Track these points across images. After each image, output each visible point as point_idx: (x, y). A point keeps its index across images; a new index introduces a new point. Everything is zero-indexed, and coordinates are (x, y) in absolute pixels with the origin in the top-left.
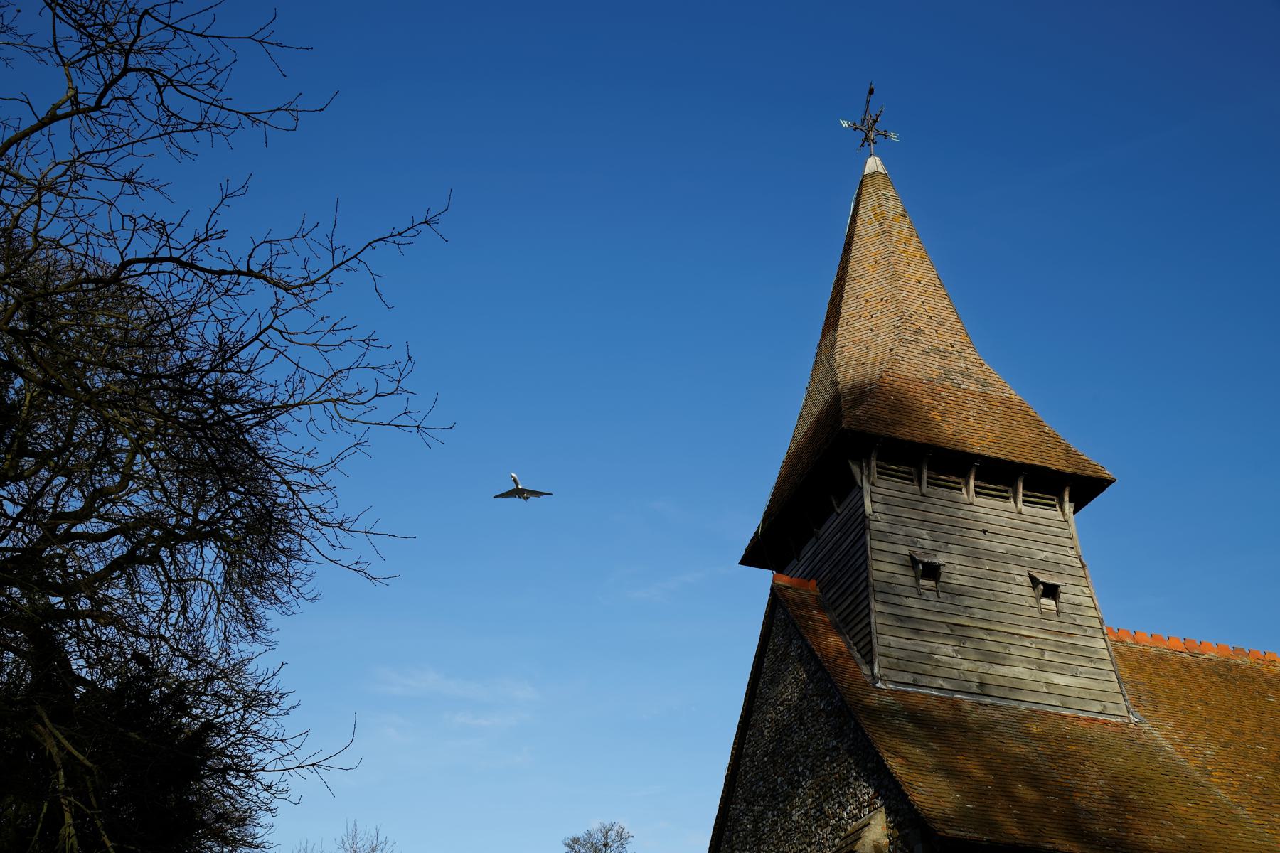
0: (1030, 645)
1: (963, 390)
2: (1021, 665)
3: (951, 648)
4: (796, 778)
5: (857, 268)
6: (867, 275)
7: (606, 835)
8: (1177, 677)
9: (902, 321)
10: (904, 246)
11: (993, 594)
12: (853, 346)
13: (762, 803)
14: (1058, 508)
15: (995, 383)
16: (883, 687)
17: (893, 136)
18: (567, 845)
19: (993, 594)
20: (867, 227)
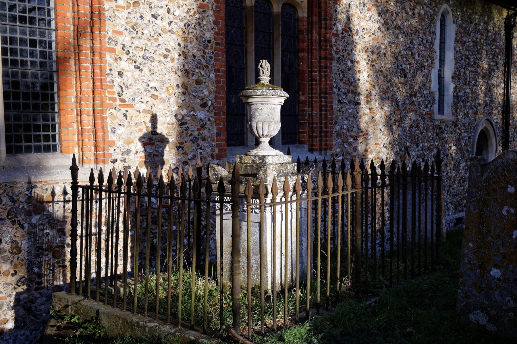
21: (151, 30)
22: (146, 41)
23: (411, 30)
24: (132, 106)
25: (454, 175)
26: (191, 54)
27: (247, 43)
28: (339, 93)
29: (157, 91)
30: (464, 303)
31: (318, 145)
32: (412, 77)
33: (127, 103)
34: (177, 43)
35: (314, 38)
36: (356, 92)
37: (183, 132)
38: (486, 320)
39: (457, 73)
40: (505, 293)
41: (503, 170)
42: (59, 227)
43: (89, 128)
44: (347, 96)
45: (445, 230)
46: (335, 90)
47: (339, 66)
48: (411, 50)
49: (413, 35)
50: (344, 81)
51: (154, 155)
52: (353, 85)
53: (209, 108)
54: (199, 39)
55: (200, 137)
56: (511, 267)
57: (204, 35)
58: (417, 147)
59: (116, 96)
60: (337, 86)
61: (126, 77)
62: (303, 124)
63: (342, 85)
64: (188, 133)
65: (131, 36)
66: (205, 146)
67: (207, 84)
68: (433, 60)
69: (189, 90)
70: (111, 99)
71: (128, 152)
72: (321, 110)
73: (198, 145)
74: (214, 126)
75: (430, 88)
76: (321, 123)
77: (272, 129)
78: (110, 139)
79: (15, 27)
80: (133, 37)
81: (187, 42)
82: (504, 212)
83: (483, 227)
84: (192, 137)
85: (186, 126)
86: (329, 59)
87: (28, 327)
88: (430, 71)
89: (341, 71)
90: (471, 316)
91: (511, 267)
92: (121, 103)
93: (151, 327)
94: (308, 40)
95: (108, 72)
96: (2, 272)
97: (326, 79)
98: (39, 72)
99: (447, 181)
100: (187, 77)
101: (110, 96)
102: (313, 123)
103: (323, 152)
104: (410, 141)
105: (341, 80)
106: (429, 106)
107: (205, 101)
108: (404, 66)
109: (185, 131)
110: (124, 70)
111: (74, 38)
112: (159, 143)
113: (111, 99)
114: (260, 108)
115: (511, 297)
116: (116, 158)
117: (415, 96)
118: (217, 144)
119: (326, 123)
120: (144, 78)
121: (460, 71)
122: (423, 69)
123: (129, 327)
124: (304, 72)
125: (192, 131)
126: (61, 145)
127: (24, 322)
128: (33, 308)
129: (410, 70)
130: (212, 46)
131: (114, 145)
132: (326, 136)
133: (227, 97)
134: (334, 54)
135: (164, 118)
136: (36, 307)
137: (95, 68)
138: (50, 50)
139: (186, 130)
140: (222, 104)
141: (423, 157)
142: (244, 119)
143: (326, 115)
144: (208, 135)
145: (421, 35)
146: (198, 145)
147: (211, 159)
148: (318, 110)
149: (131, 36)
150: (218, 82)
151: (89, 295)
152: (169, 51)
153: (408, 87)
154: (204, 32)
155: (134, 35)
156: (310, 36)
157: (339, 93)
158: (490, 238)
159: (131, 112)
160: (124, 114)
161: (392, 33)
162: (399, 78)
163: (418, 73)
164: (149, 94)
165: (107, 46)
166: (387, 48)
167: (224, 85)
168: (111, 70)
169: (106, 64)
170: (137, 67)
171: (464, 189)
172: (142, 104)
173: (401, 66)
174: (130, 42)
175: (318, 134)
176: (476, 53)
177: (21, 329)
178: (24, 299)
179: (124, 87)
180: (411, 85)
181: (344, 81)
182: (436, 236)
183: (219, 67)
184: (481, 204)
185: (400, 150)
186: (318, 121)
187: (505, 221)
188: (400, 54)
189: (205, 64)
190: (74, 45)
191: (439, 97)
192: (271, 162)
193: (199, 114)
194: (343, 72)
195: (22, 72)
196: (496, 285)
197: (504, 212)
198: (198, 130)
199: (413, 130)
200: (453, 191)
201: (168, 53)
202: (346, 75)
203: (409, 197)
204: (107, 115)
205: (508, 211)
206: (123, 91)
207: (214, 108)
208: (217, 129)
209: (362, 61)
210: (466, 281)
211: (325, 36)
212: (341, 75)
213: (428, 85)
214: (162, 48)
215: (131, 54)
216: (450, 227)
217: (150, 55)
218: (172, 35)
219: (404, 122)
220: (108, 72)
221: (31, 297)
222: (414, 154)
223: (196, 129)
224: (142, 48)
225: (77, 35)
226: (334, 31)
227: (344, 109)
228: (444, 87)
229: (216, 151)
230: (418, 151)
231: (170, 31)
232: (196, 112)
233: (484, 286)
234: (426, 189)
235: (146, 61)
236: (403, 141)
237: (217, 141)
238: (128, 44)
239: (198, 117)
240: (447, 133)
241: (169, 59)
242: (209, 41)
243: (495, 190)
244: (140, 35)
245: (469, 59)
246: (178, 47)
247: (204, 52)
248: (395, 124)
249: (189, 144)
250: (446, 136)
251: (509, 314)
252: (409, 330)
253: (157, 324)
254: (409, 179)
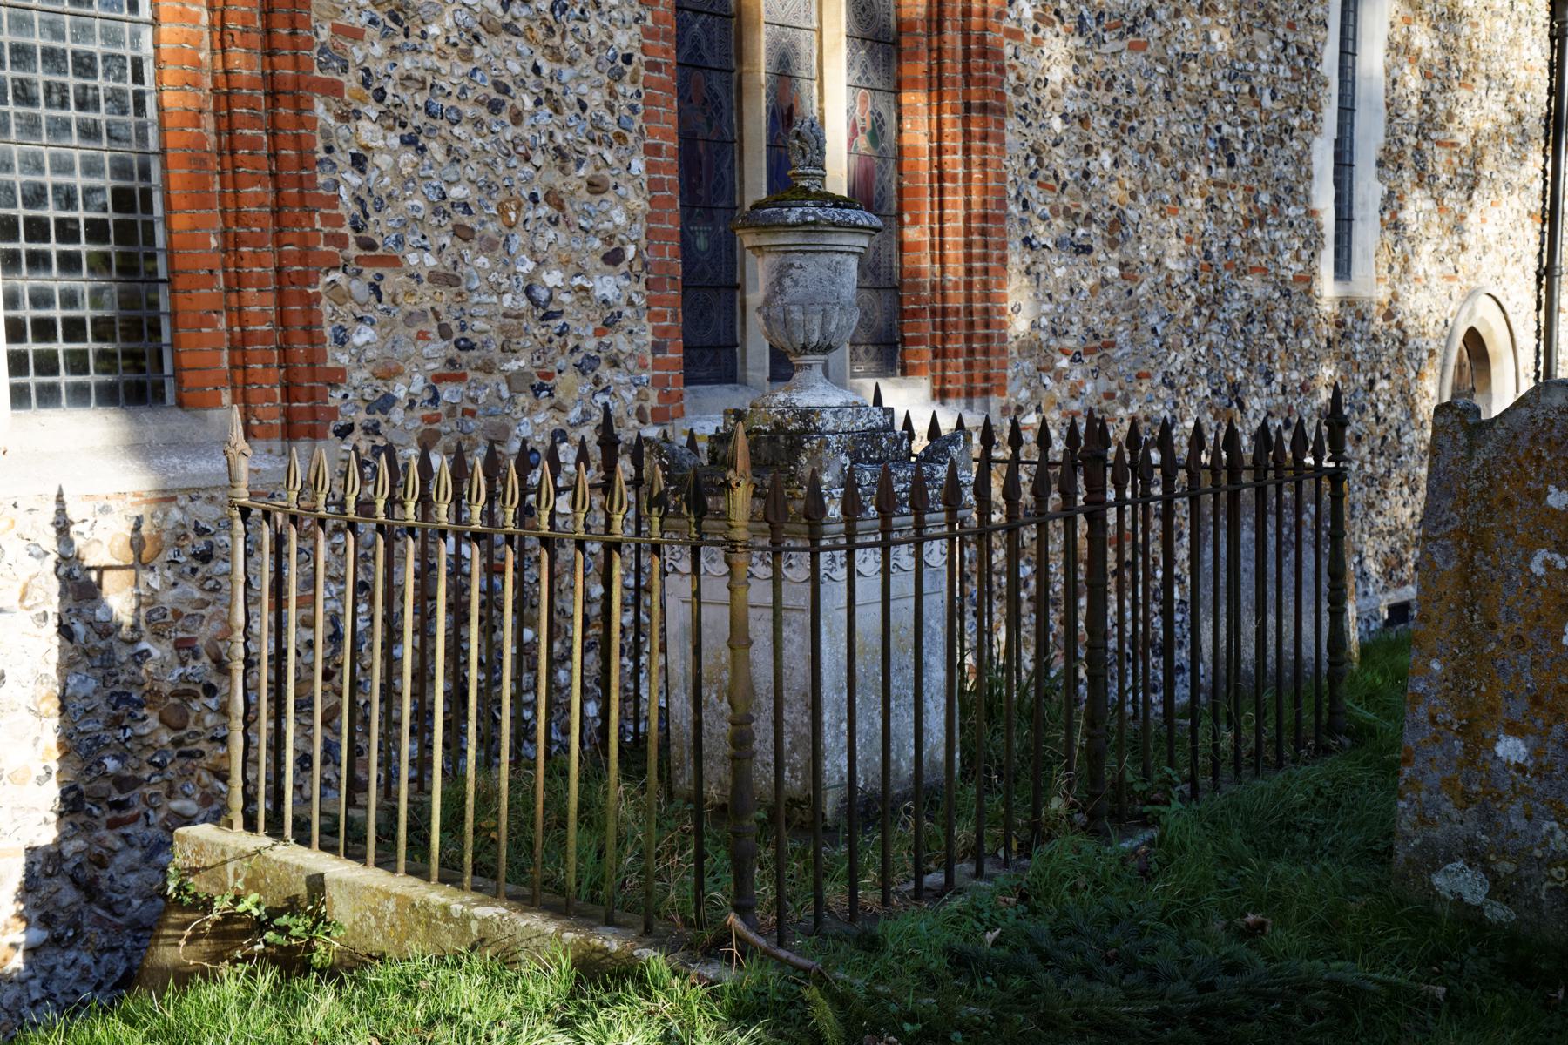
21: (449, 22)
22: (435, 58)
23: (1251, 16)
24: (394, 262)
25: (1382, 470)
26: (572, 98)
27: (740, 60)
28: (1025, 216)
29: (470, 213)
30: (1417, 841)
31: (963, 380)
32: (1253, 162)
33: (380, 251)
34: (529, 66)
35: (948, 46)
36: (1077, 215)
37: (550, 341)
38: (1483, 891)
39: (1395, 149)
40: (1542, 808)
41: (1534, 439)
42: (181, 635)
43: (265, 328)
44: (1049, 225)
45: (1354, 636)
46: (1015, 209)
47: (1026, 131)
48: (1248, 80)
49: (1256, 32)
50: (1041, 179)
51: (465, 412)
52: (1068, 190)
53: (631, 267)
54: (596, 52)
55: (602, 356)
56: (1557, 731)
57: (611, 37)
58: (1268, 384)
59: (346, 229)
60: (1019, 194)
61: (377, 172)
62: (915, 314)
63: (1034, 191)
64: (566, 344)
65: (388, 43)
66: (618, 384)
67: (621, 191)
68: (1317, 109)
69: (569, 210)
70: (333, 239)
71: (387, 402)
72: (969, 271)
73: (597, 381)
74: (645, 320)
75: (1307, 197)
76: (970, 312)
77: (833, 327)
78: (330, 364)
79: (27, 12)
80: (394, 48)
81: (560, 60)
82: (1537, 567)
83: (1472, 613)
84: (578, 357)
85: (560, 322)
86: (994, 110)
87: (88, 940)
88: (1308, 146)
89: (1032, 148)
90: (1439, 880)
91: (1557, 731)
92: (362, 253)
93: (485, 920)
94: (930, 50)
95: (321, 155)
96: (5, 774)
97: (985, 175)
98: (107, 155)
99: (1360, 489)
100: (562, 169)
101: (327, 230)
102: (944, 312)
103: (977, 402)
104: (1245, 363)
105: (1032, 176)
106: (1305, 254)
107: (616, 244)
108: (1226, 129)
109: (557, 339)
110: (368, 148)
111: (212, 49)
112: (479, 375)
113: (333, 239)
114: (797, 264)
115: (1558, 821)
116: (349, 421)
117: (1262, 223)
118: (655, 378)
119: (986, 311)
120: (431, 172)
121: (1402, 144)
122: (1286, 137)
123: (419, 922)
124: (915, 150)
125: (579, 337)
126: (179, 382)
127: (76, 926)
128: (104, 884)
129: (1245, 143)
130: (636, 72)
131: (343, 381)
132: (986, 352)
133: (682, 233)
134: (1009, 93)
135: (495, 299)
136: (111, 879)
137: (280, 141)
138: (138, 87)
139: (559, 335)
140: (670, 254)
141: (1286, 414)
142: (733, 301)
143: (985, 284)
144: (627, 348)
145: (1280, 31)
146: (597, 381)
147: (636, 423)
148: (961, 270)
149: (388, 43)
150: (654, 185)
151: (288, 831)
152: (505, 90)
153: (1240, 197)
154: (612, 28)
155: (399, 40)
156: (935, 39)
157: (1025, 216)
158: (1493, 645)
159: (393, 281)
160: (371, 284)
161: (1188, 26)
162: (1210, 168)
163: (1271, 150)
164: (448, 224)
165: (317, 73)
166: (1176, 73)
167: (676, 195)
168: (329, 149)
169: (314, 129)
170: (409, 141)
171: (1413, 515)
172: (427, 255)
173: (1219, 129)
174: (386, 62)
175: (962, 345)
176: (1456, 83)
177: (67, 948)
178: (76, 853)
179: (369, 201)
180: (1248, 189)
181: (1041, 179)
182: (1329, 649)
183: (657, 140)
184: (1465, 544)
185: (1214, 392)
186: (962, 305)
187: (1538, 594)
188: (1216, 93)
189: (617, 129)
190: (213, 73)
191: (1337, 228)
192: (830, 427)
193: (598, 284)
194: (1037, 152)
195: (52, 156)
196: (1513, 785)
197: (1537, 567)
198: (598, 333)
199: (1256, 329)
200: (1379, 520)
201: (501, 97)
202: (1046, 162)
203: (1247, 534)
204: (320, 289)
205: (1548, 565)
206: (367, 216)
207: (645, 265)
208: (655, 331)
209: (1098, 115)
210: (1422, 774)
211: (982, 39)
212: (1032, 161)
213: (1301, 189)
214: (483, 80)
215: (389, 100)
216: (1370, 634)
217: (447, 103)
218: (515, 39)
219: (1225, 305)
220: (321, 155)
221: (97, 849)
222: (1258, 407)
223: (590, 331)
224: (424, 82)
225: (222, 40)
226: (1008, 23)
227: (1042, 268)
228: (1351, 195)
229: (653, 400)
230: (1271, 395)
231: (507, 27)
232: (589, 279)
233: (1475, 788)
234: (1299, 510)
235: (438, 122)
236: (1222, 364)
237: (654, 368)
238: (378, 68)
239: (597, 294)
240: (1361, 340)
241: (505, 116)
242: (628, 59)
243: (1508, 503)
244: (414, 40)
245: (1432, 105)
246: (533, 77)
247: (613, 93)
248: (1199, 314)
249: (570, 377)
250: (1359, 348)
251: (1554, 872)
252: (1251, 918)
253: (502, 911)
254: (1246, 477)
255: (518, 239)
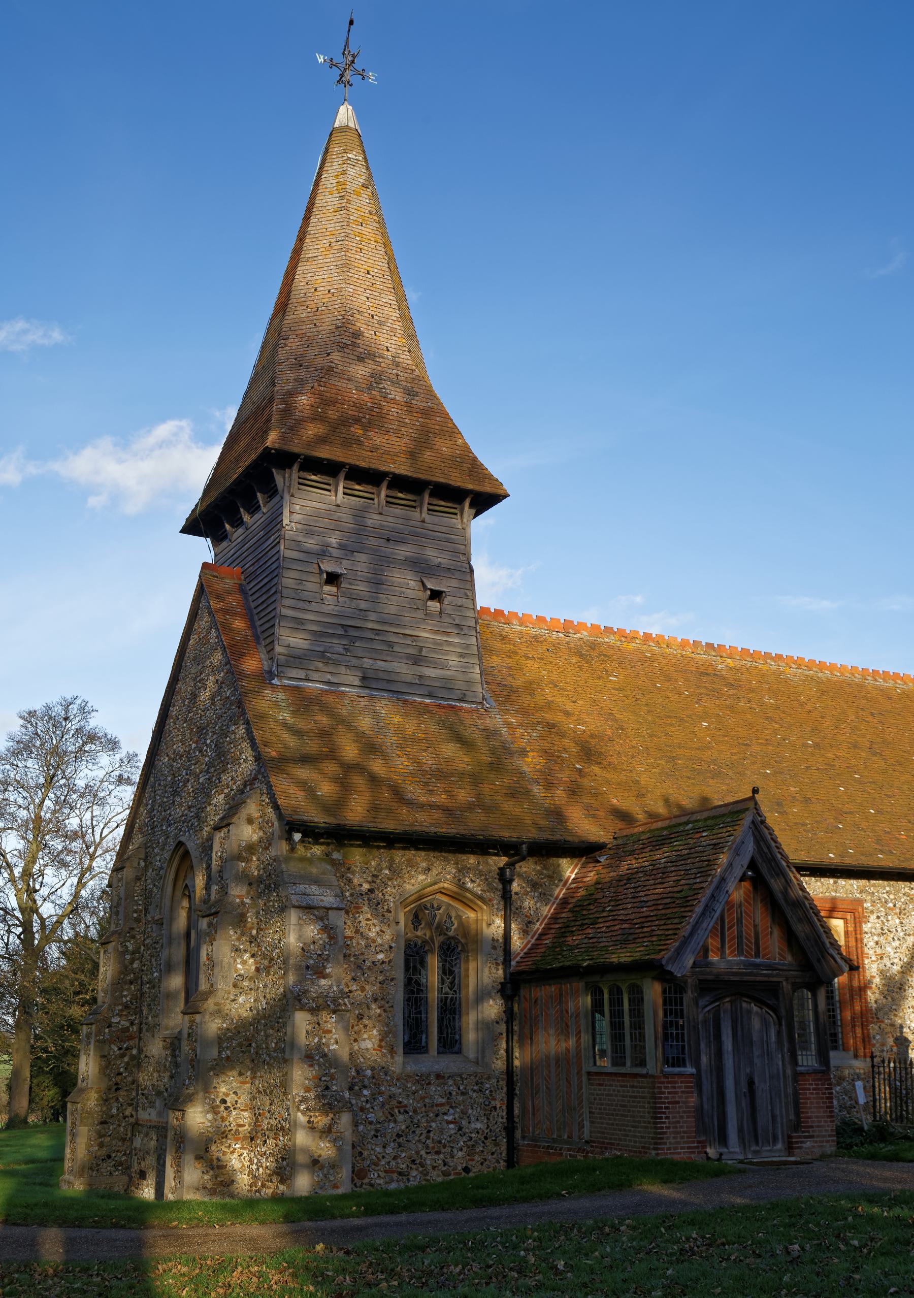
0: (411, 643)
1: (389, 401)
2: (400, 661)
3: (340, 646)
4: (205, 748)
5: (312, 247)
6: (320, 258)
7: (67, 709)
8: (542, 659)
9: (344, 321)
10: (360, 227)
11: (387, 598)
12: (296, 340)
13: (179, 761)
14: (459, 517)
15: (421, 391)
16: (278, 683)
17: (372, 77)
18: (22, 717)
19: (387, 598)
20: (327, 200)
24: (883, 1022)
113: (873, 1018)
255: (906, 1017)
